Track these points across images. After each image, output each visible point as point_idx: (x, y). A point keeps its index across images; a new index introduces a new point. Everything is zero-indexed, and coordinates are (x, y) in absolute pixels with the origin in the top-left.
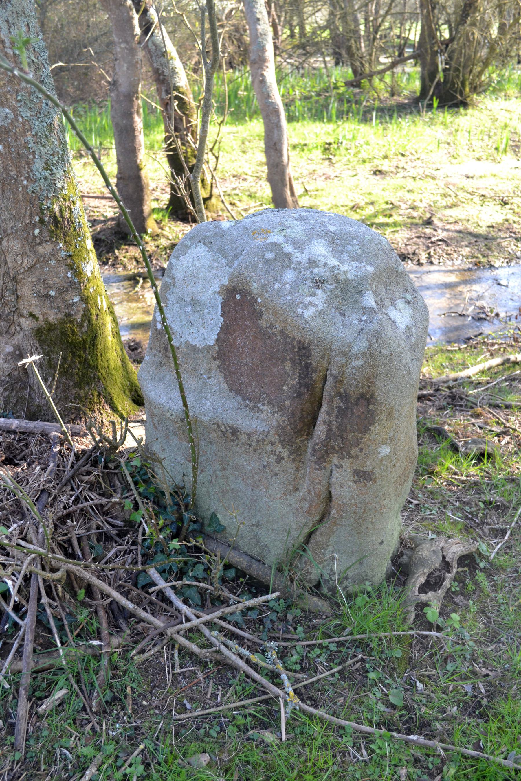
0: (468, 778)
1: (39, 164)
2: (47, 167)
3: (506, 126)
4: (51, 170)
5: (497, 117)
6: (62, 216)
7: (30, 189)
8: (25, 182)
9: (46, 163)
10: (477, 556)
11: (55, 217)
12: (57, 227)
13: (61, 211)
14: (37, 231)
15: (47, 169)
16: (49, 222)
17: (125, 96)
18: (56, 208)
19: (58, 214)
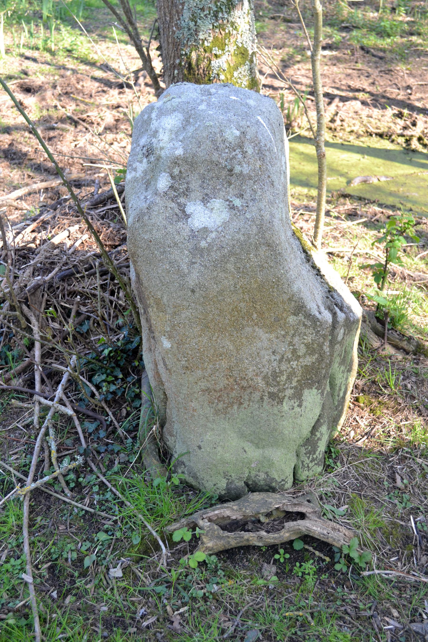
0: (320, 639)
1: (187, 15)
2: (194, 19)
3: (102, 119)
4: (196, 22)
5: (327, 256)
6: (197, 65)
7: (176, 35)
8: (174, 29)
9: (193, 15)
10: (121, 90)
11: (190, 64)
12: (189, 73)
13: (198, 60)
14: (176, 72)
15: (192, 20)
16: (184, 66)
17: (257, 20)
18: (194, 55)
19: (194, 62)
